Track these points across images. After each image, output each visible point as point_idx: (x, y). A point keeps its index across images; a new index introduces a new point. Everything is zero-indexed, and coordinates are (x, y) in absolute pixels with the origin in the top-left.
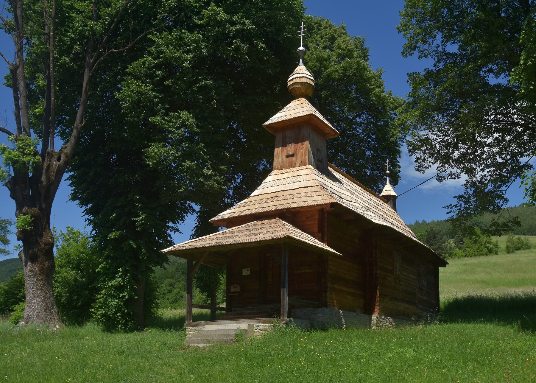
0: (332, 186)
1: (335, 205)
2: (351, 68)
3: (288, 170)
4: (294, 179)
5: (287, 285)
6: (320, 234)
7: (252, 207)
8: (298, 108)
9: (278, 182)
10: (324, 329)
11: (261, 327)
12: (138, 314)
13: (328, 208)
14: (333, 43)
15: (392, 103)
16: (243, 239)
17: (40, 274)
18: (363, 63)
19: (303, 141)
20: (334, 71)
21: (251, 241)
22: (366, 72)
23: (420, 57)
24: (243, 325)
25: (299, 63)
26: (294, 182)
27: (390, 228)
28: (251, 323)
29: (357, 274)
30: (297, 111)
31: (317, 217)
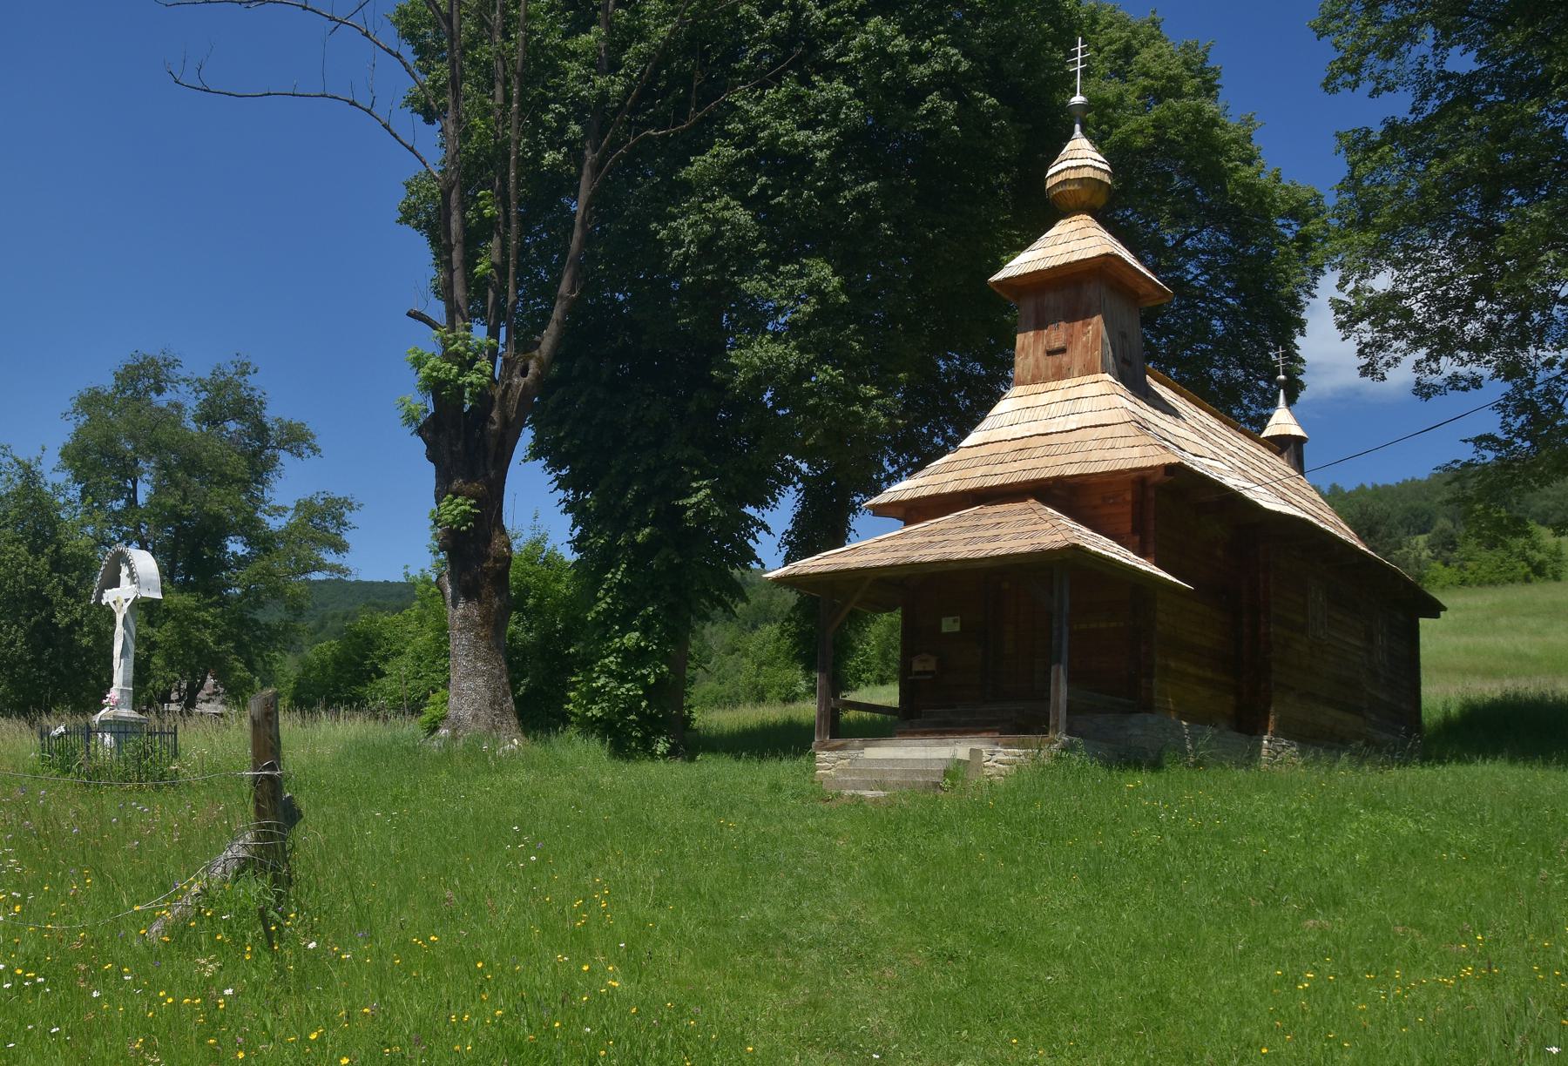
0: (1157, 421)
1: (1177, 471)
2: (1178, 122)
3: (1052, 385)
4: (1068, 407)
5: (1065, 657)
6: (1137, 538)
7: (969, 473)
8: (1074, 241)
9: (1028, 414)
10: (1156, 766)
11: (999, 757)
12: (654, 723)
13: (1160, 476)
14: (1128, 63)
15: (1283, 201)
16: (960, 550)
17: (482, 626)
18: (1210, 108)
19: (1087, 315)
20: (1135, 132)
21: (982, 554)
22: (1217, 131)
23: (1375, 92)
24: (958, 749)
25: (1073, 132)
26: (1065, 416)
27: (1294, 517)
28: (976, 747)
29: (1219, 635)
30: (1071, 246)
31: (1129, 497)
